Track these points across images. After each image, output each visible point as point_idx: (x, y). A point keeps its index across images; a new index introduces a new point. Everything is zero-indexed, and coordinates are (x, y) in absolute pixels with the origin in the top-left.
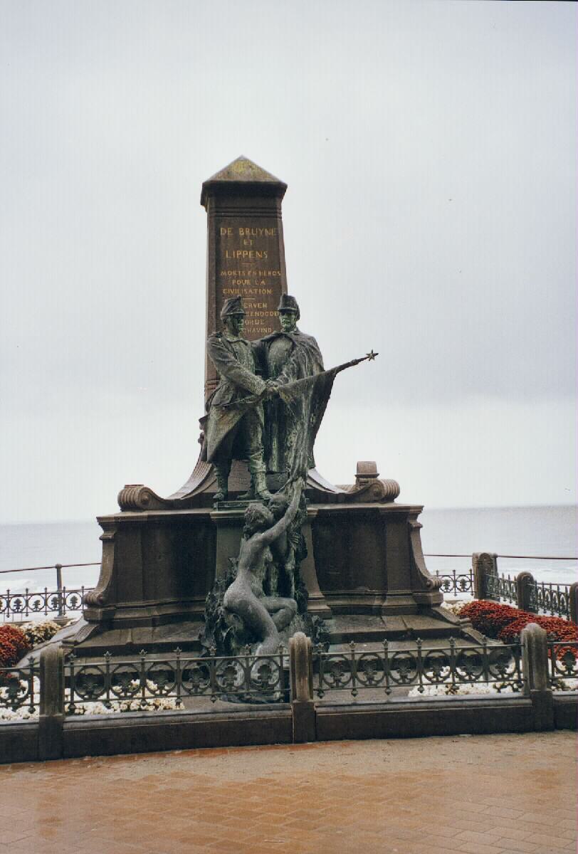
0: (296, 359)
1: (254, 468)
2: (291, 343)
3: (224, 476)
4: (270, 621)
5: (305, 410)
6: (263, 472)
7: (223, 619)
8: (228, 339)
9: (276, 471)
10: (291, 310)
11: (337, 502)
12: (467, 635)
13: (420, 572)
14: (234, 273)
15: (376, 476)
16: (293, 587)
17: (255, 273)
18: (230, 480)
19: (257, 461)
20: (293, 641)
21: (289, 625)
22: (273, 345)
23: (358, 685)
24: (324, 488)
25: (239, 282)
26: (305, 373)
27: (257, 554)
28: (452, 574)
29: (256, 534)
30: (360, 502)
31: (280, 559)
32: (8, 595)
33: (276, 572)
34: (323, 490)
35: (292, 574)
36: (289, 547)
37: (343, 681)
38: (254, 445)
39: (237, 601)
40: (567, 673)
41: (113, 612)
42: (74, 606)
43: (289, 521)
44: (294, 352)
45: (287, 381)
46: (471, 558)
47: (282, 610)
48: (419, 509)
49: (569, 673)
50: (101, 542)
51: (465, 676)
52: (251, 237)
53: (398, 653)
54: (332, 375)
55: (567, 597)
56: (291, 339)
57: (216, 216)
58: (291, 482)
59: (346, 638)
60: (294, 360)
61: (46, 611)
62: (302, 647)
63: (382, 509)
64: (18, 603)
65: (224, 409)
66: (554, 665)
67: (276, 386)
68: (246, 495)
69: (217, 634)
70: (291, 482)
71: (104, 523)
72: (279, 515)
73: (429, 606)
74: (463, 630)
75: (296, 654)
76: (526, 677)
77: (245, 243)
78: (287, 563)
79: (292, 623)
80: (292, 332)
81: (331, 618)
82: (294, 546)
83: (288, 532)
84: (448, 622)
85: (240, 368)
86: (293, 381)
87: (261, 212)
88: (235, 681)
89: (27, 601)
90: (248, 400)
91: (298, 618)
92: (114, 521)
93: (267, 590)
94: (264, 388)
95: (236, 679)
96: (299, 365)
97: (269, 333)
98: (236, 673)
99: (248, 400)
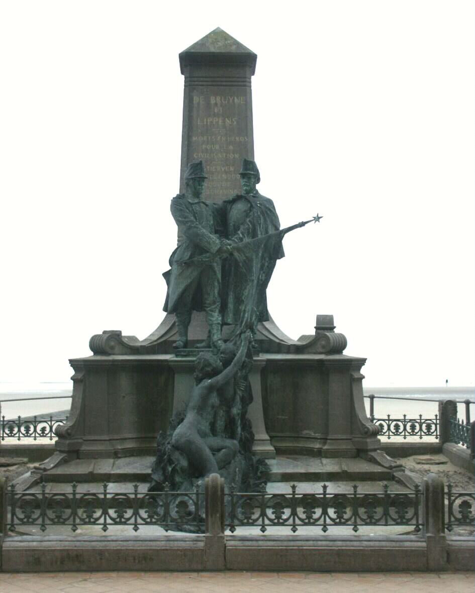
0: (252, 220)
1: (211, 320)
2: (249, 205)
3: (185, 324)
4: (212, 460)
5: (256, 266)
6: (218, 324)
7: (169, 456)
8: (190, 201)
9: (231, 323)
10: (250, 174)
11: (288, 352)
12: (397, 479)
13: (360, 420)
15: (332, 328)
16: (239, 429)
18: (190, 329)
19: (213, 314)
20: (208, 481)
21: (229, 463)
22: (234, 206)
23: (139, 521)
24: (279, 339)
25: (209, 147)
26: (259, 233)
27: (205, 398)
29: (204, 381)
30: (309, 353)
31: (227, 403)
32: (421, 420)
33: (223, 416)
34: (278, 341)
35: (237, 418)
36: (235, 393)
37: (406, 517)
38: (210, 299)
39: (183, 440)
40: (118, 520)
41: (81, 444)
42: (397, 431)
43: (235, 369)
44: (251, 214)
45: (241, 239)
47: (224, 450)
50: (72, 382)
51: (275, 519)
53: (117, 494)
56: (249, 201)
57: (190, 85)
58: (240, 334)
59: (286, 478)
60: (250, 221)
61: (51, 437)
62: (215, 487)
63: (327, 360)
64: (397, 427)
65: (183, 265)
66: (13, 514)
67: (230, 245)
68: (203, 344)
69: (164, 469)
70: (240, 334)
71: (74, 363)
72: (226, 363)
73: (366, 451)
74: (394, 474)
75: (210, 493)
76: (424, 522)
77: (216, 111)
78: (233, 407)
79: (233, 461)
80: (252, 194)
81: (274, 458)
82: (239, 392)
83: (235, 379)
84: (379, 464)
85: (197, 228)
86: (247, 240)
88: (344, 515)
90: (205, 258)
91: (240, 458)
93: (214, 431)
94: (219, 247)
96: (254, 226)
97: (232, 194)
98: (470, 508)
99: (205, 258)
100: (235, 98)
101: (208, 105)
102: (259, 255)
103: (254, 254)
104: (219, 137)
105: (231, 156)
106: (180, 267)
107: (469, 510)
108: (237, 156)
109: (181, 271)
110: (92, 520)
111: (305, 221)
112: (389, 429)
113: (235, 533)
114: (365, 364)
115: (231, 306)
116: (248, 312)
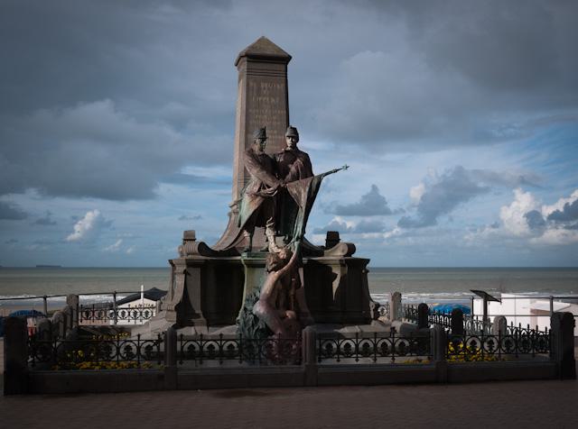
28: (137, 338)
48: (368, 261)
54: (320, 178)
89: (141, 313)
105: (274, 123)
107: (236, 349)
112: (141, 315)
113: (322, 363)
115: (282, 224)
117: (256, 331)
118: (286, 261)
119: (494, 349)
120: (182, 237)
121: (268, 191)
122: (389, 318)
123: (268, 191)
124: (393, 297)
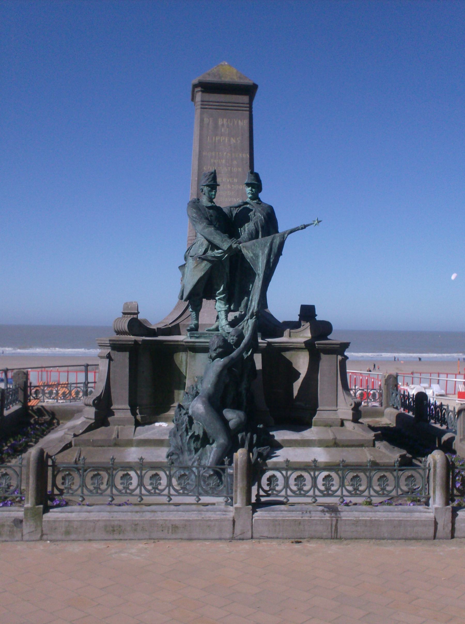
14: (213, 154)
17: (229, 154)
46: (224, 311)
47: (234, 420)
49: (328, 492)
52: (228, 126)
55: (413, 400)
65: (198, 259)
87: (232, 106)
92: (133, 343)
95: (131, 484)
100: (239, 121)
101: (216, 127)
102: (264, 252)
103: (260, 251)
104: (225, 153)
105: (235, 170)
106: (194, 261)
108: (240, 170)
109: (196, 265)
110: (99, 491)
111: (306, 224)
114: (349, 347)
116: (255, 301)
117: (191, 437)
118: (237, 344)
119: (131, 487)
120: (122, 310)
121: (217, 253)
122: (381, 405)
123: (217, 253)
124: (386, 381)
